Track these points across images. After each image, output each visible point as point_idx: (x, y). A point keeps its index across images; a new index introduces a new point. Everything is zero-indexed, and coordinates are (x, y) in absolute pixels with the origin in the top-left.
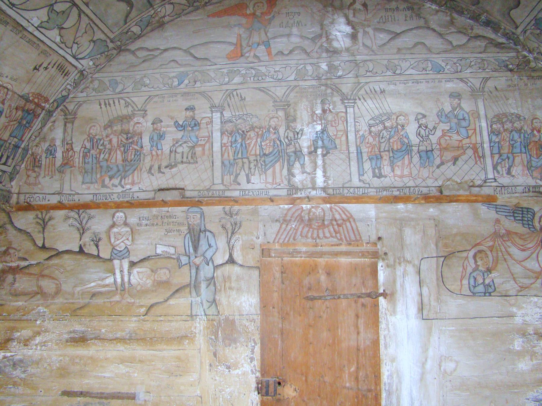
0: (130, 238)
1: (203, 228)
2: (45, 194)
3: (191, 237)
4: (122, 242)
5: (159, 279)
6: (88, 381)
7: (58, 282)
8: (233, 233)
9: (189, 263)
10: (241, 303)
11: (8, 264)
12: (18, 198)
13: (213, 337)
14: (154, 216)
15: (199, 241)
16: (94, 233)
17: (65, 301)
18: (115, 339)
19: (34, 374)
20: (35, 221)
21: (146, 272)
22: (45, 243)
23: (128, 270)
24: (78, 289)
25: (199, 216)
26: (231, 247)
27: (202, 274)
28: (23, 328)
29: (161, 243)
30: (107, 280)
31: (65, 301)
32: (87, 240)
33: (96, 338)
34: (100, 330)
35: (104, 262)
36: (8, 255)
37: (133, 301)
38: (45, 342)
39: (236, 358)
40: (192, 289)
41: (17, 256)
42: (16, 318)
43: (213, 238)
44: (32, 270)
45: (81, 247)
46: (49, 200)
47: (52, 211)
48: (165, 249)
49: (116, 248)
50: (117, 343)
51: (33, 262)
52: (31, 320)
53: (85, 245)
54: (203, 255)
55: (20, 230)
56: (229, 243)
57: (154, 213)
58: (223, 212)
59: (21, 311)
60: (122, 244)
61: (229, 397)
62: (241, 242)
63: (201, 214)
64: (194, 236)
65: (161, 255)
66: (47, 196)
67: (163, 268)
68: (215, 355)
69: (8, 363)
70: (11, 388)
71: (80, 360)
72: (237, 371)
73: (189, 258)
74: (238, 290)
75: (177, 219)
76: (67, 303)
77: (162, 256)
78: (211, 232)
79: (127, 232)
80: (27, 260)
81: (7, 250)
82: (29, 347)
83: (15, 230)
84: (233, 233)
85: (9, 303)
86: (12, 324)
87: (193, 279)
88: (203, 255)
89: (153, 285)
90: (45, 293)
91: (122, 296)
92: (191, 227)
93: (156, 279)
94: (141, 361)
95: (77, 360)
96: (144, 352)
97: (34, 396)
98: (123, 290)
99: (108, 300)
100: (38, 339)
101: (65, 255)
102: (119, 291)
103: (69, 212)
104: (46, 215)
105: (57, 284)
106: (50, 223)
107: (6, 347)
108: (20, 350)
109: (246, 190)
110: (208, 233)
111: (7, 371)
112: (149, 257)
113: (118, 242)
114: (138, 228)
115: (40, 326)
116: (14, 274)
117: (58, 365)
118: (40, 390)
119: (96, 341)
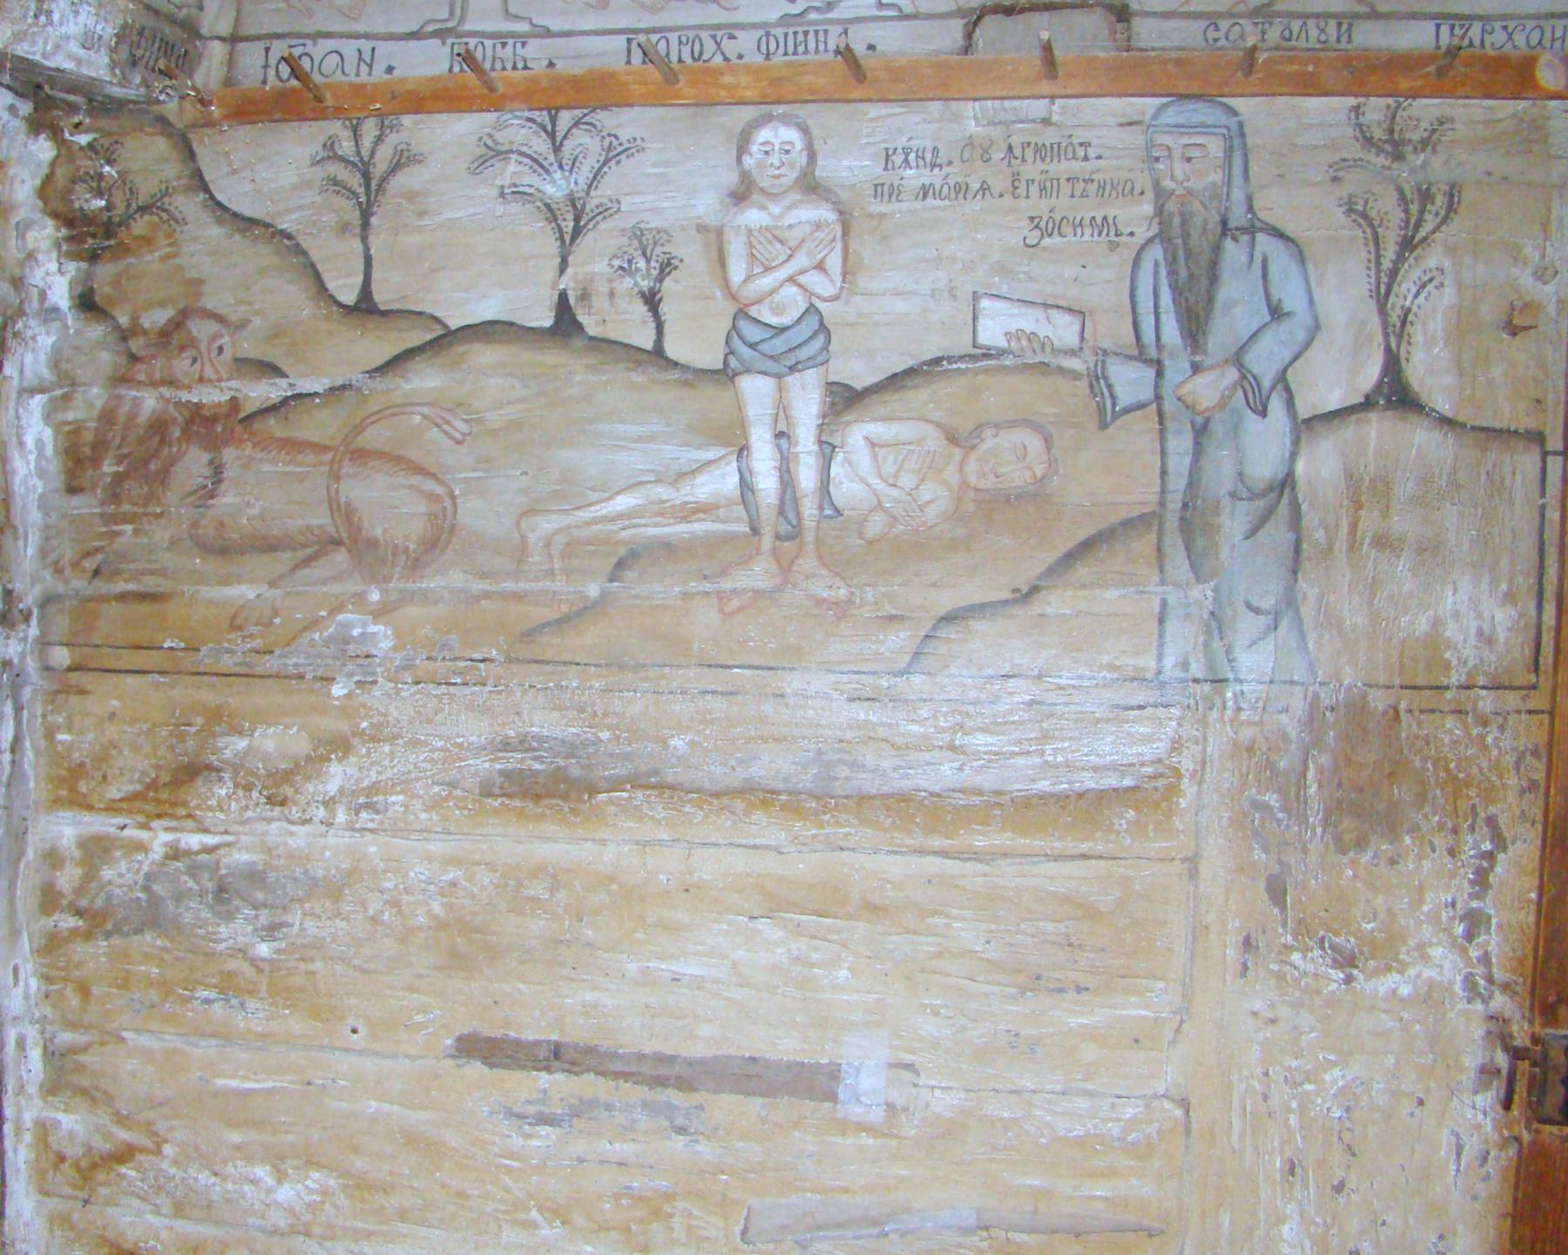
0: (834, 261)
1: (1238, 217)
2: (367, 36)
3: (1172, 262)
4: (791, 279)
5: (988, 483)
6: (589, 997)
7: (439, 490)
8: (1408, 245)
9: (1158, 398)
10: (1436, 623)
11: (184, 396)
12: (231, 62)
13: (1272, 799)
14: (970, 143)
15: (1214, 278)
16: (638, 234)
17: (479, 586)
18: (740, 792)
19: (318, 945)
20: (319, 173)
21: (920, 441)
22: (374, 287)
23: (821, 427)
24: (548, 524)
25: (1215, 146)
26: (1394, 318)
27: (1220, 470)
28: (263, 717)
29: (1004, 290)
30: (700, 479)
31: (479, 586)
32: (600, 267)
33: (636, 782)
34: (664, 743)
35: (686, 384)
36: (183, 348)
37: (843, 593)
38: (374, 789)
39: (1391, 913)
40: (1167, 540)
41: (228, 354)
42: (227, 663)
43: (1294, 270)
44: (320, 425)
45: (563, 306)
46: (390, 70)
47: (407, 120)
48: (1029, 321)
49: (753, 312)
50: (748, 812)
51: (307, 385)
52: (301, 677)
53: (584, 296)
54: (1237, 359)
55: (245, 224)
56: (1382, 300)
57: (972, 127)
58: (1350, 131)
59: (255, 629)
60: (791, 290)
61: (1337, 1113)
62: (1449, 296)
63: (1228, 139)
64: (1189, 254)
65: (1002, 352)
66: (383, 47)
67: (1012, 424)
68: (1277, 892)
69: (191, 883)
70: (207, 1001)
71: (552, 890)
72: (1392, 979)
73: (1160, 374)
74: (1421, 550)
75: (1093, 164)
76: (487, 595)
77: (1008, 361)
78: (1281, 235)
79: (818, 226)
80: (284, 375)
81: (178, 323)
82: (295, 813)
83: (220, 222)
84: (1408, 245)
85: (189, 589)
86: (207, 695)
87: (1178, 483)
88: (1237, 359)
89: (956, 515)
90: (373, 543)
91: (785, 567)
92: (1171, 206)
93: (973, 479)
94: (874, 910)
95: (538, 890)
96: (895, 867)
97: (322, 1048)
98: (789, 538)
99: (708, 586)
100: (337, 775)
101: (478, 347)
102: (767, 542)
103: (498, 127)
104: (379, 139)
105: (433, 498)
106: (399, 182)
107: (185, 804)
108: (248, 821)
109: (1471, 18)
110: (1264, 242)
111: (188, 918)
112: (937, 361)
113: (766, 282)
114: (876, 207)
115: (348, 708)
116: (214, 444)
117: (436, 907)
118: (352, 1022)
119: (639, 794)
